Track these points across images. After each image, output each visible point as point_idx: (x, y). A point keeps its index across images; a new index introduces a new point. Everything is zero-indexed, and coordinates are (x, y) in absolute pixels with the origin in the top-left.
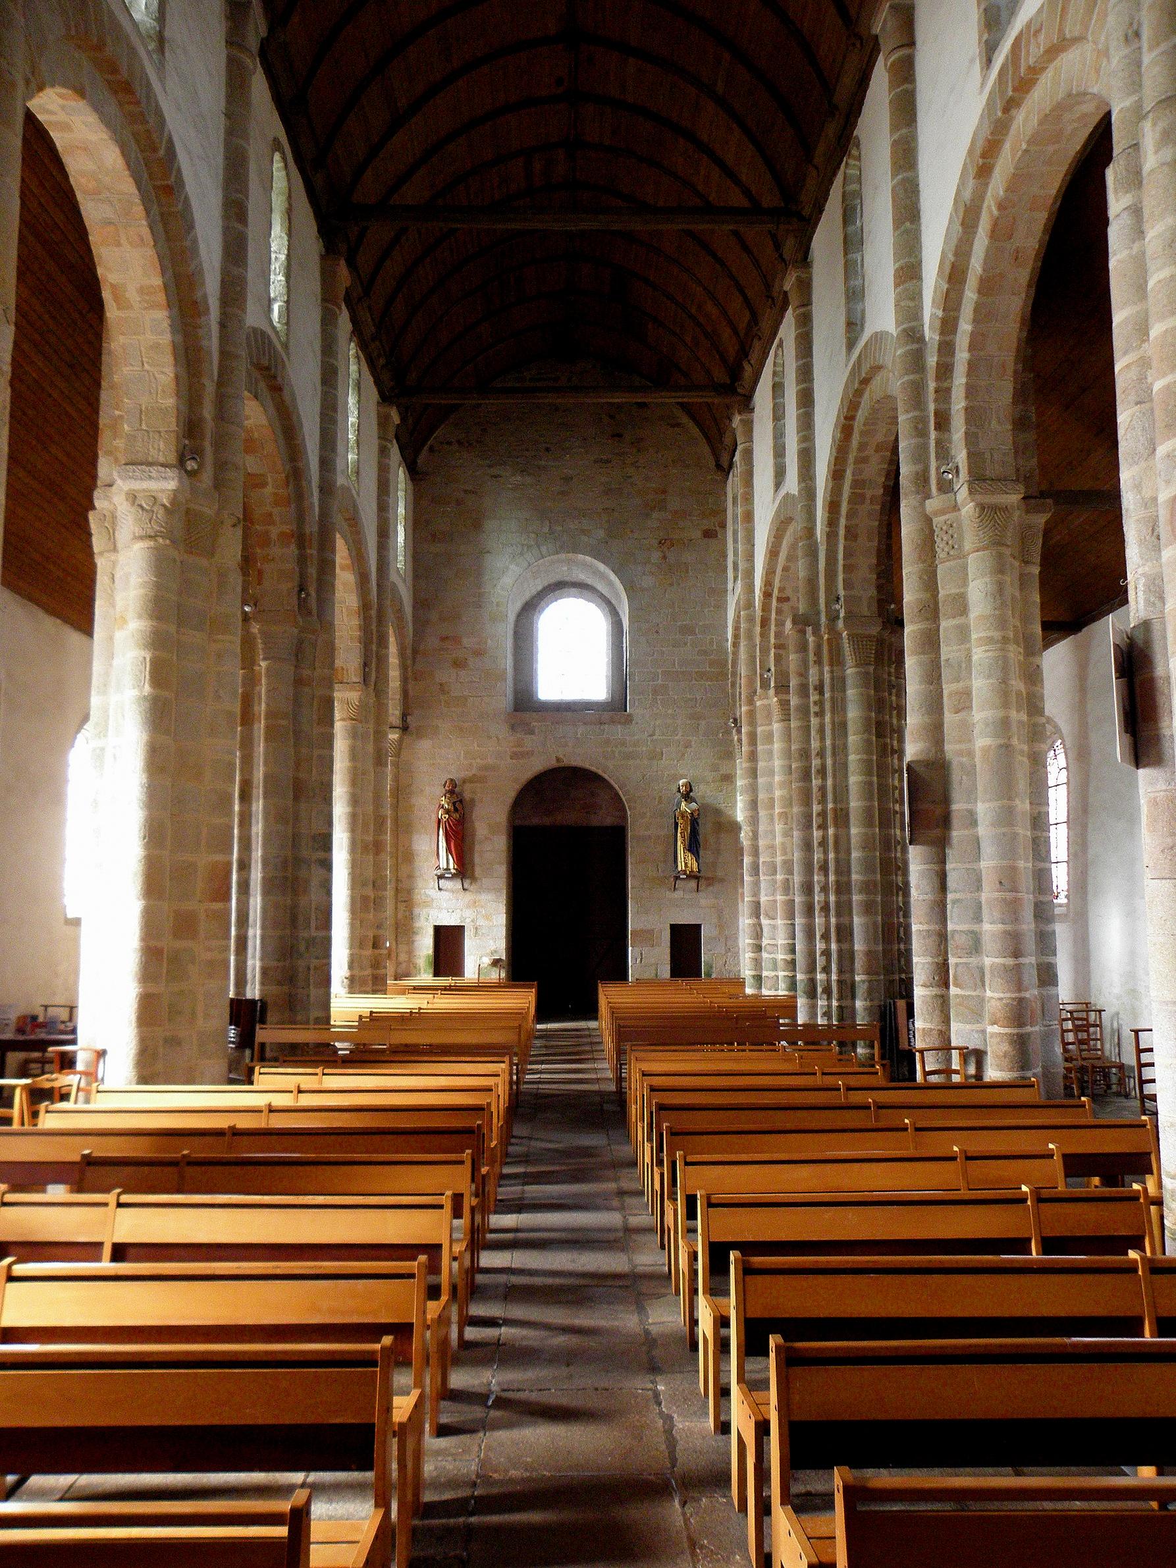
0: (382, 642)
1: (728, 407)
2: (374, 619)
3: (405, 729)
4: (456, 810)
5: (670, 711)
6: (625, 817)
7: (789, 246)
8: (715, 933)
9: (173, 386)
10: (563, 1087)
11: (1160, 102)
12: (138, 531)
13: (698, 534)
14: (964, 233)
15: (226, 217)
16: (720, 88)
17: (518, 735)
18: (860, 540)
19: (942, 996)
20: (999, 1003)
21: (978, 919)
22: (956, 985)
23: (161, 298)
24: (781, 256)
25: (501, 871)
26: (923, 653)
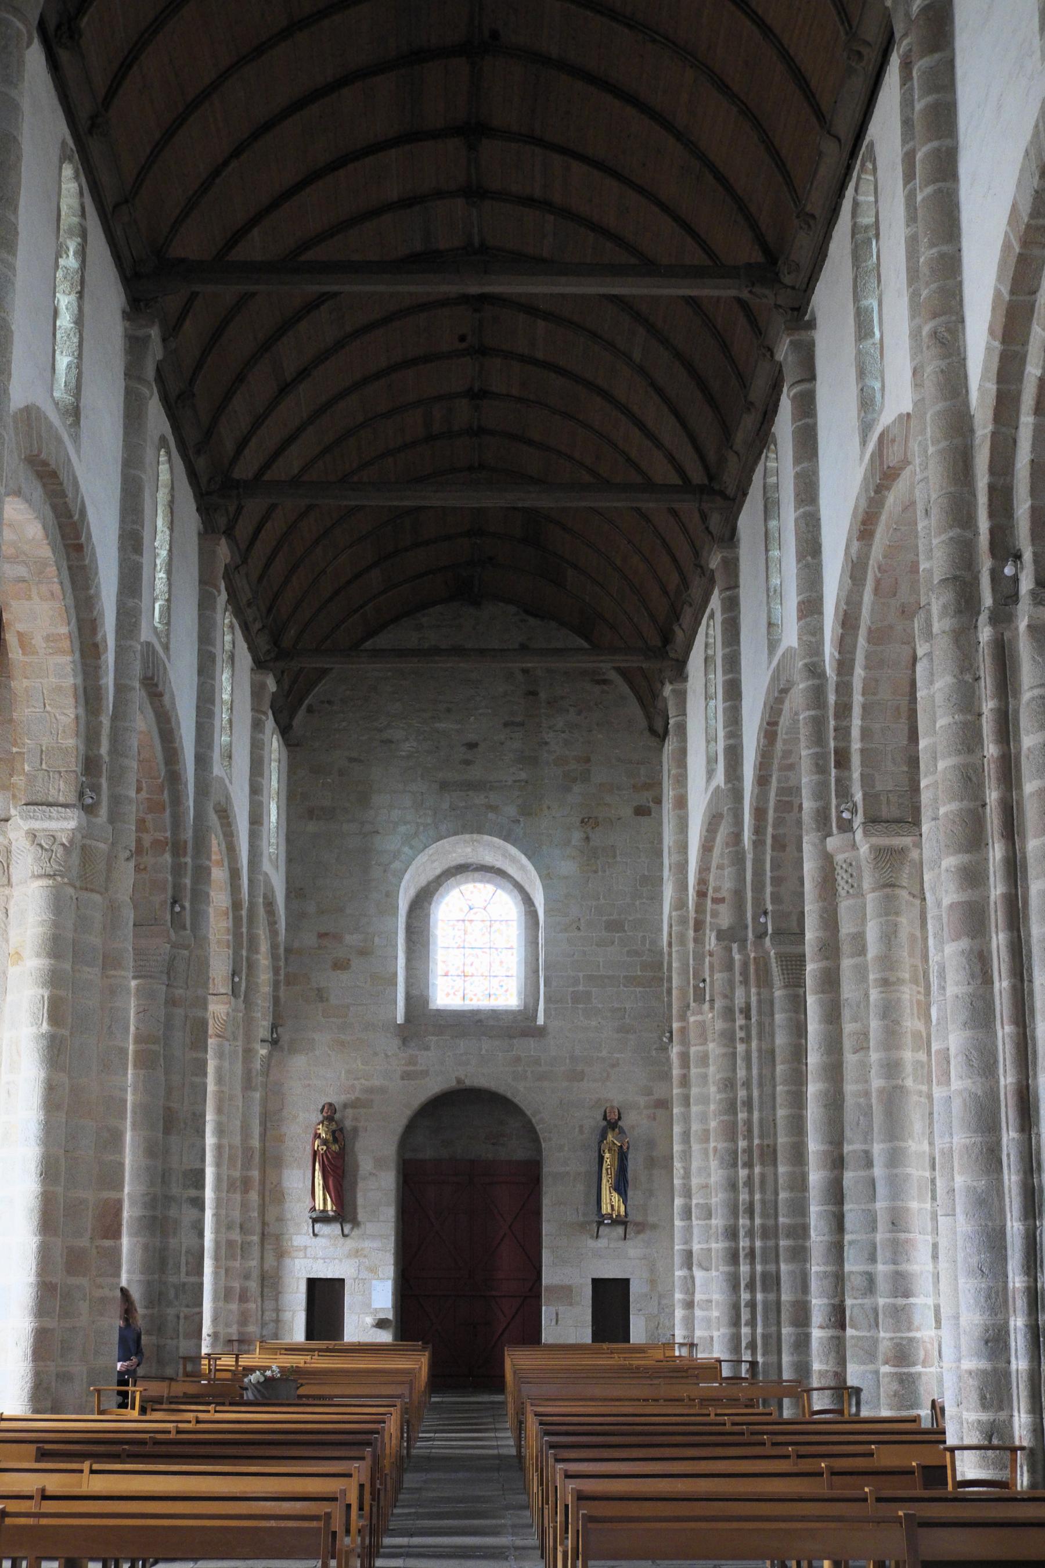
0: (253, 945)
1: (661, 671)
2: (245, 920)
3: (275, 1043)
4: (335, 1140)
5: (594, 1023)
6: (539, 1150)
7: (715, 520)
8: (645, 1289)
9: (73, 726)
10: (457, 1451)
11: (948, 579)
12: (38, 870)
13: (627, 812)
14: (854, 585)
15: (122, 549)
16: (637, 356)
17: (410, 1051)
18: (788, 849)
19: (838, 1338)
20: (889, 1343)
21: (873, 1259)
22: (852, 1327)
23: (66, 644)
24: (707, 528)
25: (389, 1213)
26: (823, 992)
